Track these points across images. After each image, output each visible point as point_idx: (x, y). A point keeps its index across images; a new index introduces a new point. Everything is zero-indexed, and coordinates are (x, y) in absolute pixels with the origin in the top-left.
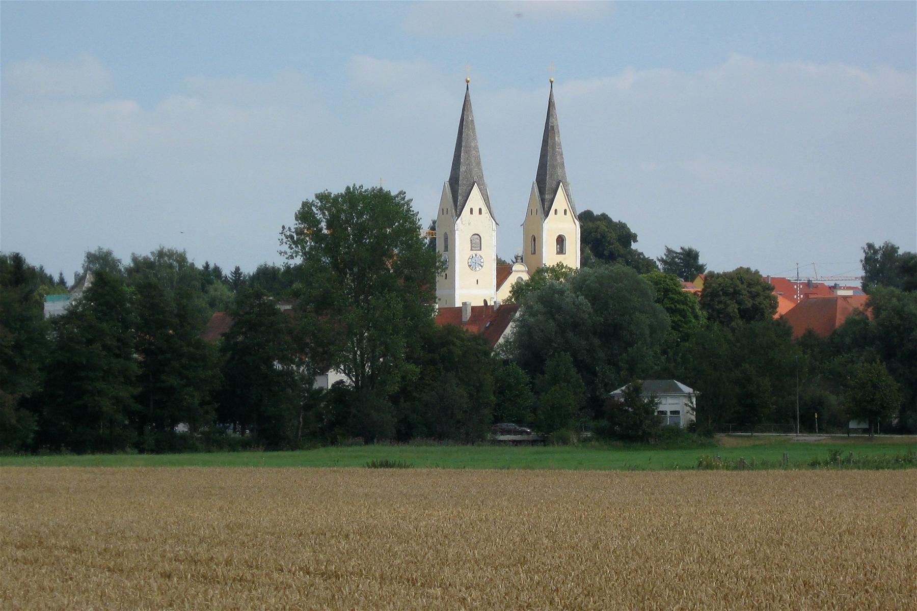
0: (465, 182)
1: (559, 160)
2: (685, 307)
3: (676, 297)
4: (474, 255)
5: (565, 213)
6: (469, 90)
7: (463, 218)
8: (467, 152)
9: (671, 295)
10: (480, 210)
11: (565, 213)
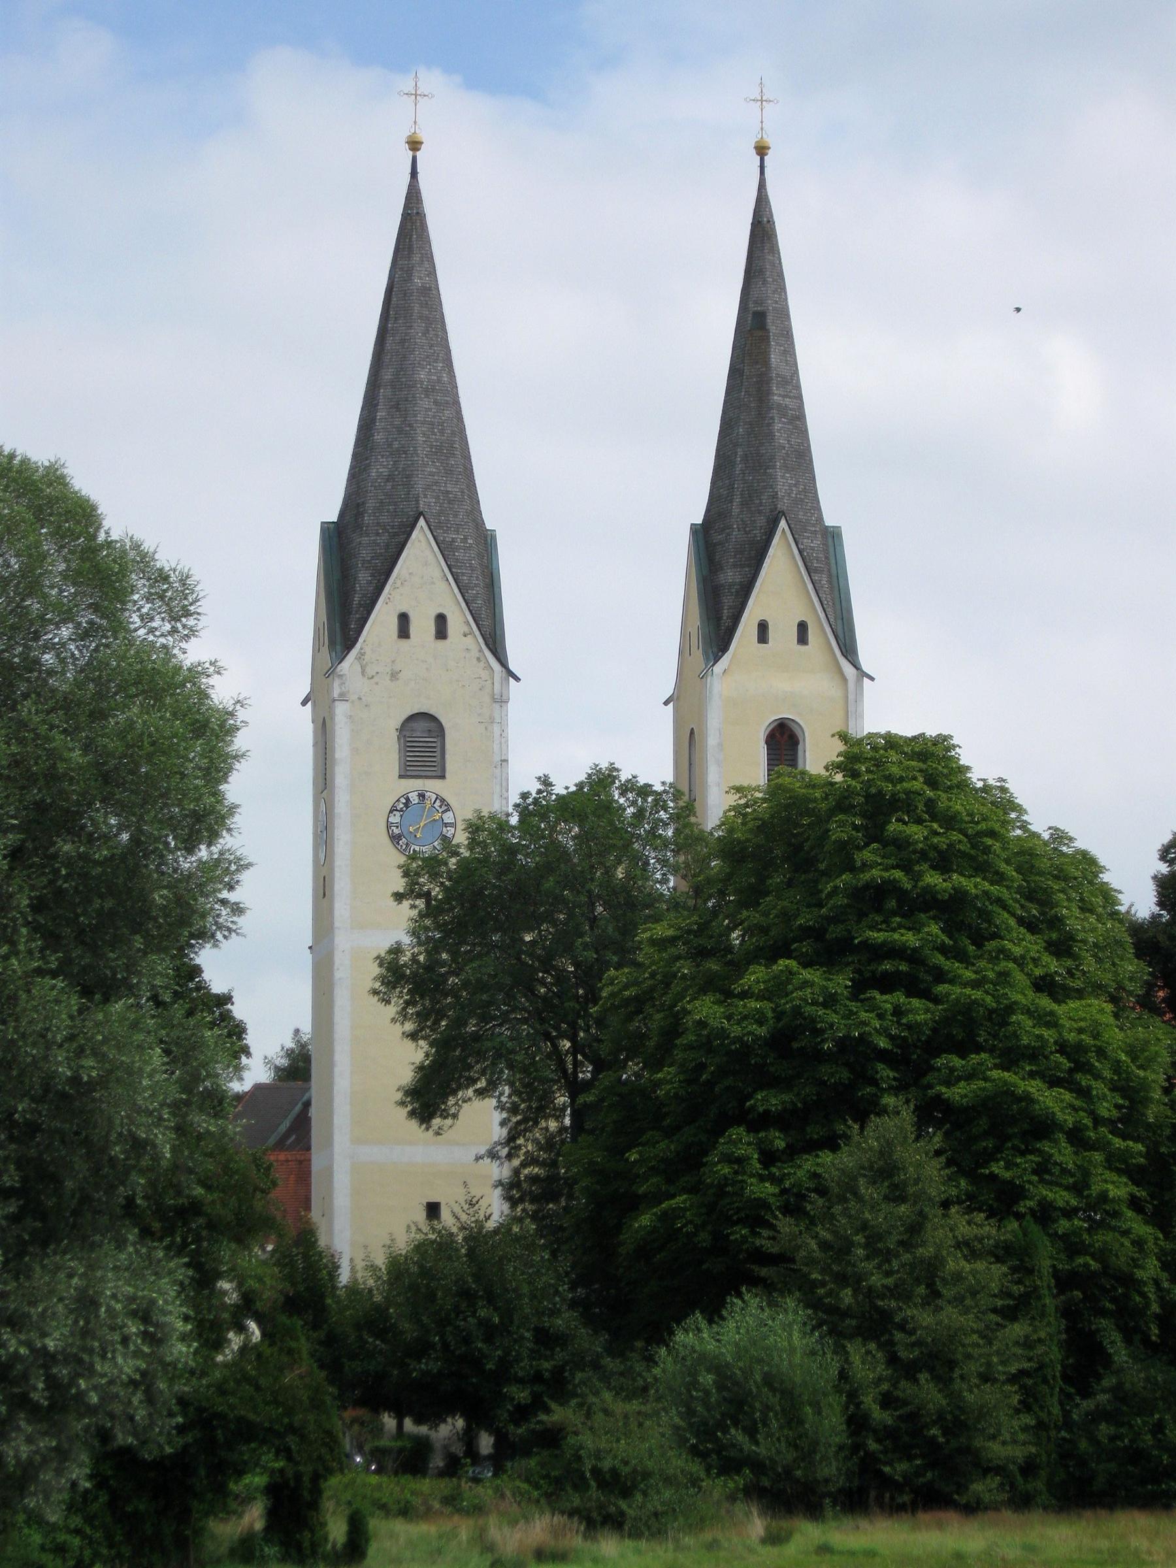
0: (385, 519)
1: (781, 439)
2: (972, 885)
3: (916, 832)
4: (414, 797)
5: (802, 638)
6: (420, 177)
7: (368, 650)
8: (398, 409)
9: (894, 827)
10: (441, 620)
11: (802, 638)
